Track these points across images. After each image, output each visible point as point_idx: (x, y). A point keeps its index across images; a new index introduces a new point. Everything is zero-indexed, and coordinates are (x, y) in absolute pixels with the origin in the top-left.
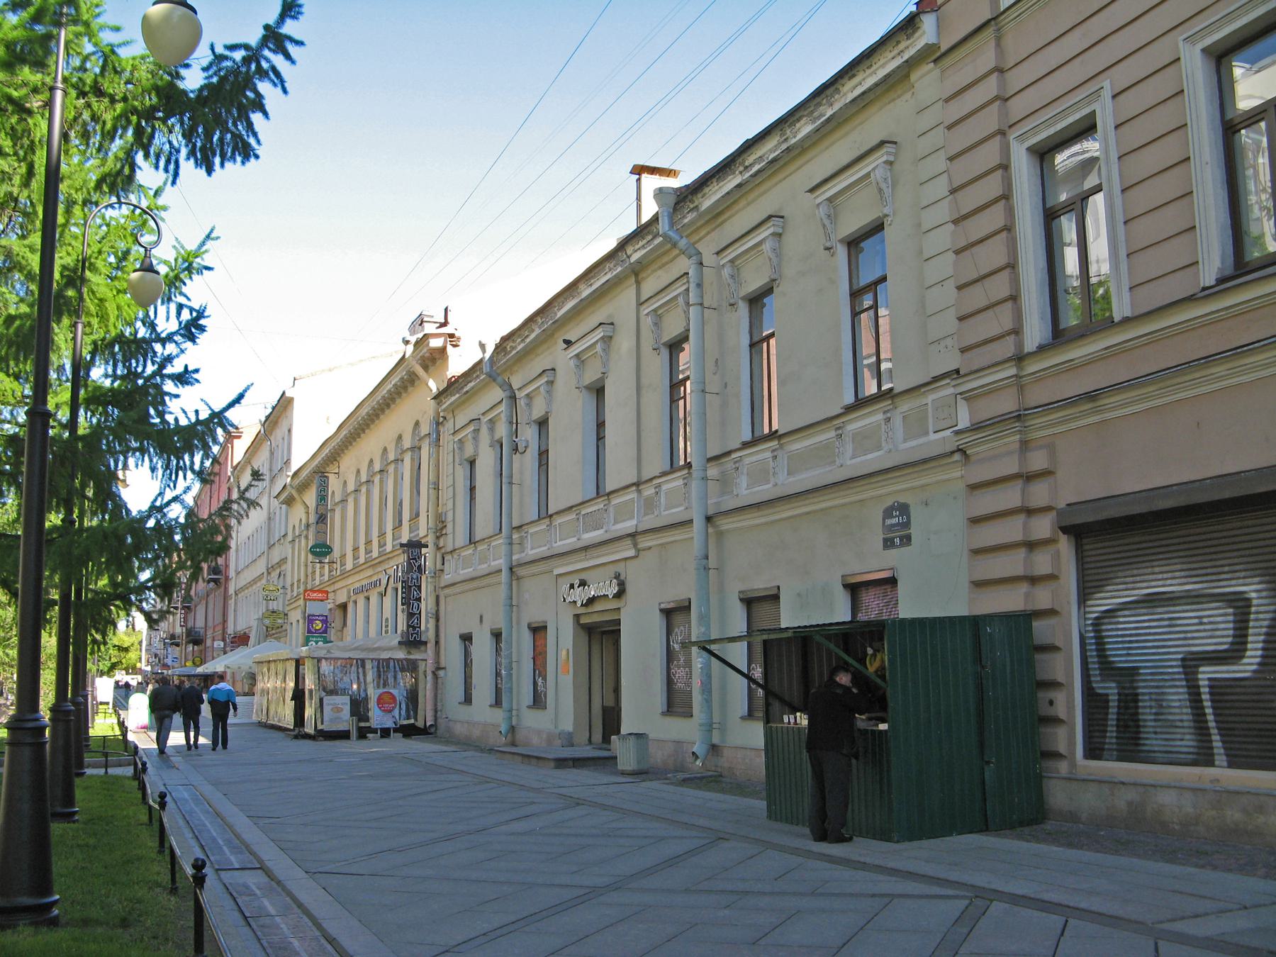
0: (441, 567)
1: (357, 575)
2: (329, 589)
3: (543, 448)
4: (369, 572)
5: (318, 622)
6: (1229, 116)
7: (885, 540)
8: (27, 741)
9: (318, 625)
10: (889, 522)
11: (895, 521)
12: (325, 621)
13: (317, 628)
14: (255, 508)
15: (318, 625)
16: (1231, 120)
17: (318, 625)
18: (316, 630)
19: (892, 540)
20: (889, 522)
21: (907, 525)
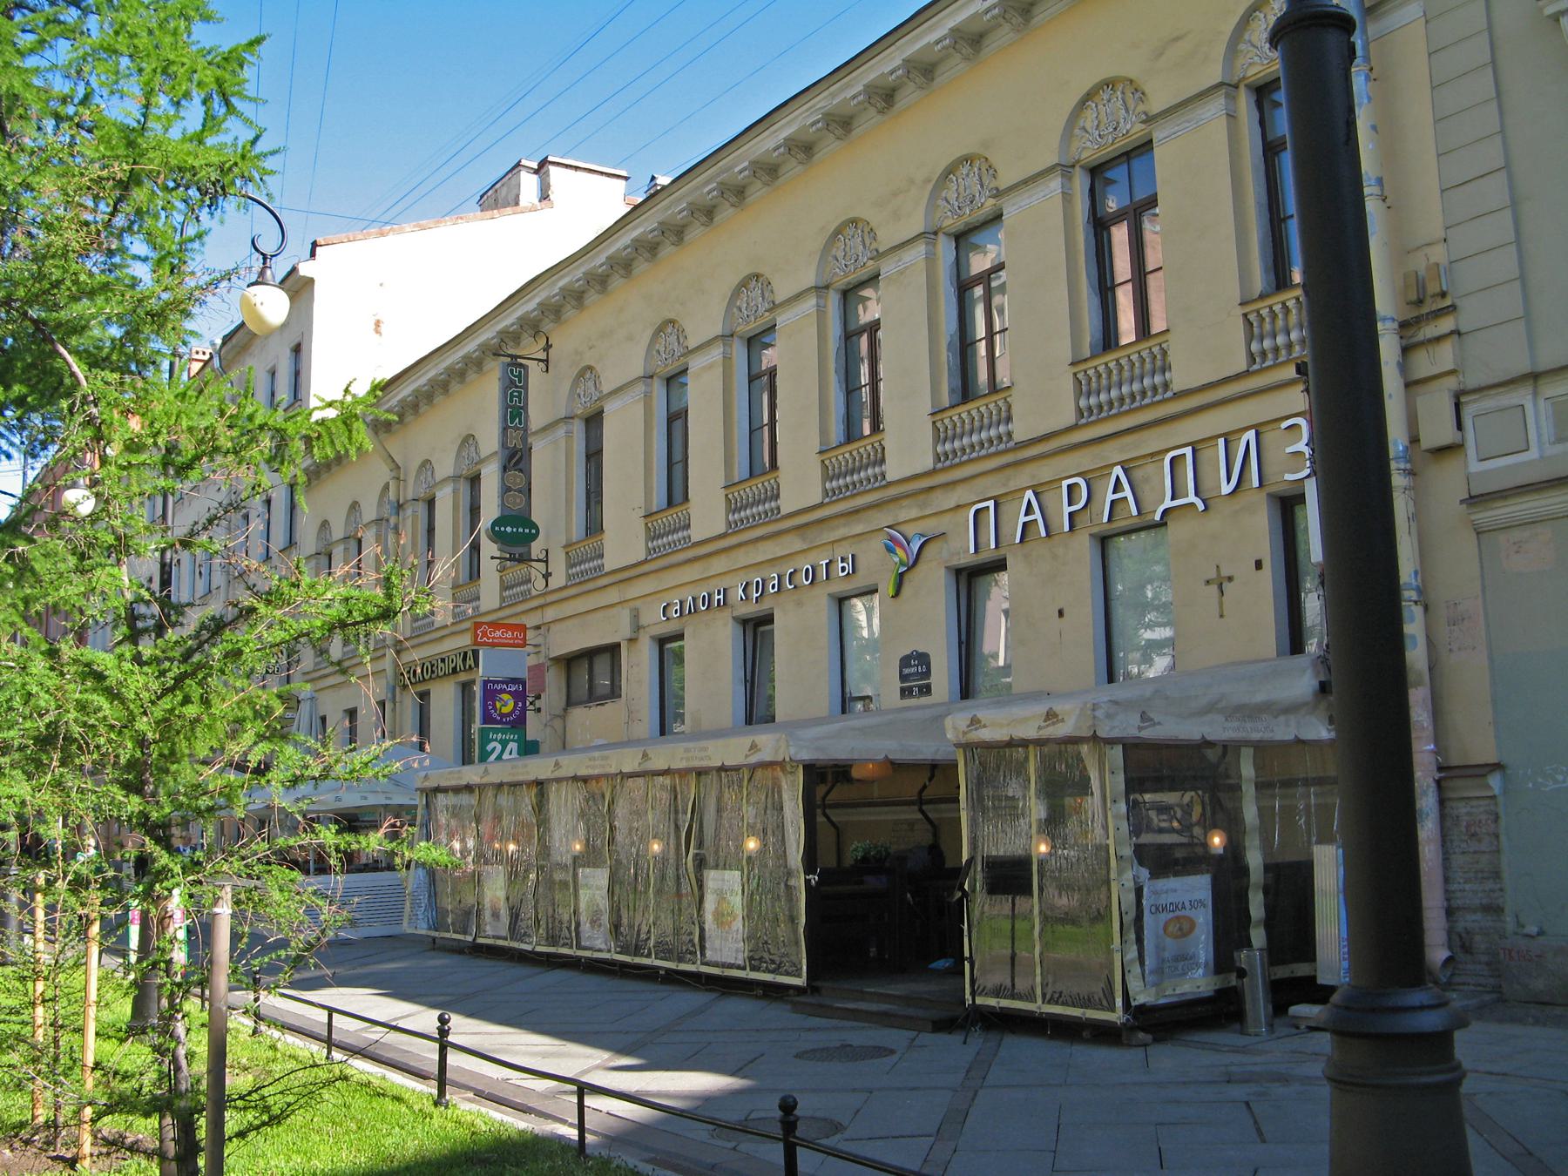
0: (1447, 435)
1: (698, 566)
2: (530, 621)
3: (593, 449)
4: (794, 543)
5: (505, 697)
6: (1270, 138)
7: (903, 690)
8: (1139, 970)
9: (507, 704)
10: (906, 671)
11: (913, 670)
12: (519, 696)
13: (506, 710)
14: (203, 303)
15: (507, 704)
16: (1272, 141)
17: (505, 704)
18: (503, 715)
19: (910, 690)
20: (906, 671)
21: (927, 674)
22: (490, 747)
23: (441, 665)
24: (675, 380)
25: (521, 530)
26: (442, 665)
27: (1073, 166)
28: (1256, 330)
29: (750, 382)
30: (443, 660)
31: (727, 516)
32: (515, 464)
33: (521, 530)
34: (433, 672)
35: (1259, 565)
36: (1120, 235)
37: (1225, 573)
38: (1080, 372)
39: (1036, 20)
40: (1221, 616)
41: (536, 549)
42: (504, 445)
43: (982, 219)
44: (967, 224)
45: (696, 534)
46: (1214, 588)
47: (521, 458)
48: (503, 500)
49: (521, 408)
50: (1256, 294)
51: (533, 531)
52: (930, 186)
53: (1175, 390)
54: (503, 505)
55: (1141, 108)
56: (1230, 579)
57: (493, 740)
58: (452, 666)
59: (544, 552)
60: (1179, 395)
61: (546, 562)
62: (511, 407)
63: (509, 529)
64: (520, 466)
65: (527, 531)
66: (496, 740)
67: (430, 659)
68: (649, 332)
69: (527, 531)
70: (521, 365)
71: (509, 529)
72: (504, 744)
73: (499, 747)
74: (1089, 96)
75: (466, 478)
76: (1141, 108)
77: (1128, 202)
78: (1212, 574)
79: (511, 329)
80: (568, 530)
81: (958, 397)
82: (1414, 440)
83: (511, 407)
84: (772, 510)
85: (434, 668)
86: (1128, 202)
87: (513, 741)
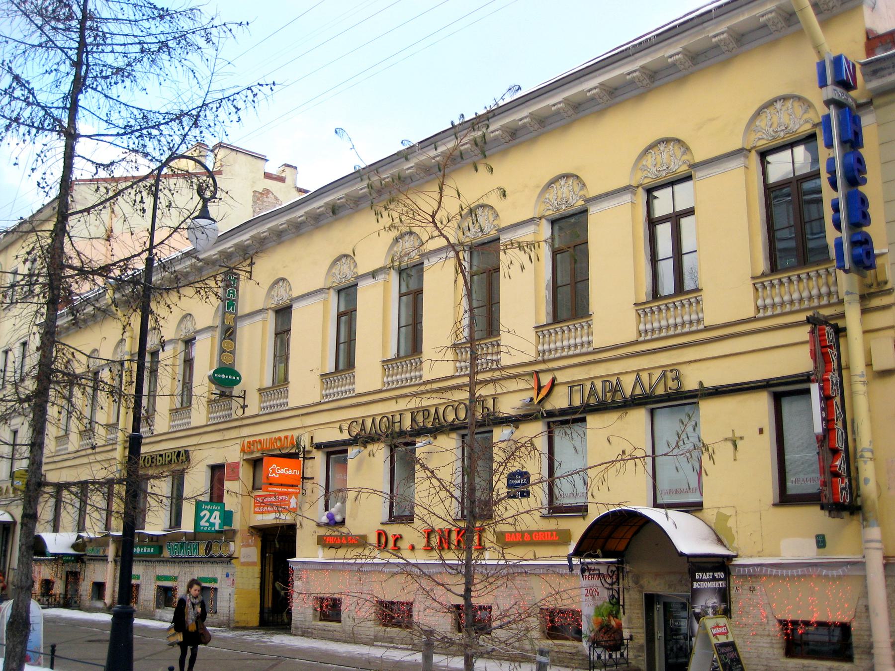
1: (237, 430)
10: (512, 482)
20: (512, 482)
22: (202, 514)
23: (159, 458)
24: (189, 342)
25: (230, 377)
26: (161, 458)
27: (638, 187)
28: (541, 340)
29: (400, 297)
30: (161, 455)
31: (321, 392)
32: (230, 335)
33: (230, 377)
34: (152, 462)
35: (761, 431)
36: (664, 232)
37: (738, 434)
38: (647, 308)
39: (322, 222)
40: (735, 460)
41: (236, 390)
42: (223, 322)
43: (571, 213)
44: (561, 214)
45: (359, 388)
46: (730, 445)
47: (232, 333)
48: (220, 357)
49: (234, 301)
50: (759, 274)
51: (238, 378)
52: (539, 190)
53: (706, 325)
54: (220, 361)
55: (582, 193)
56: (741, 438)
57: (204, 509)
58: (168, 459)
59: (243, 392)
60: (707, 329)
61: (244, 398)
62: (228, 299)
63: (223, 376)
64: (232, 337)
65: (234, 378)
66: (206, 509)
67: (151, 454)
68: (331, 260)
69: (234, 378)
70: (236, 274)
71: (223, 376)
72: (211, 512)
73: (208, 514)
74: (771, 104)
75: (182, 341)
76: (582, 193)
77: (792, 176)
78: (730, 435)
79: (229, 250)
80: (261, 380)
81: (410, 351)
82: (869, 364)
83: (228, 299)
84: (416, 377)
85: (154, 460)
86: (792, 176)
87: (217, 510)
